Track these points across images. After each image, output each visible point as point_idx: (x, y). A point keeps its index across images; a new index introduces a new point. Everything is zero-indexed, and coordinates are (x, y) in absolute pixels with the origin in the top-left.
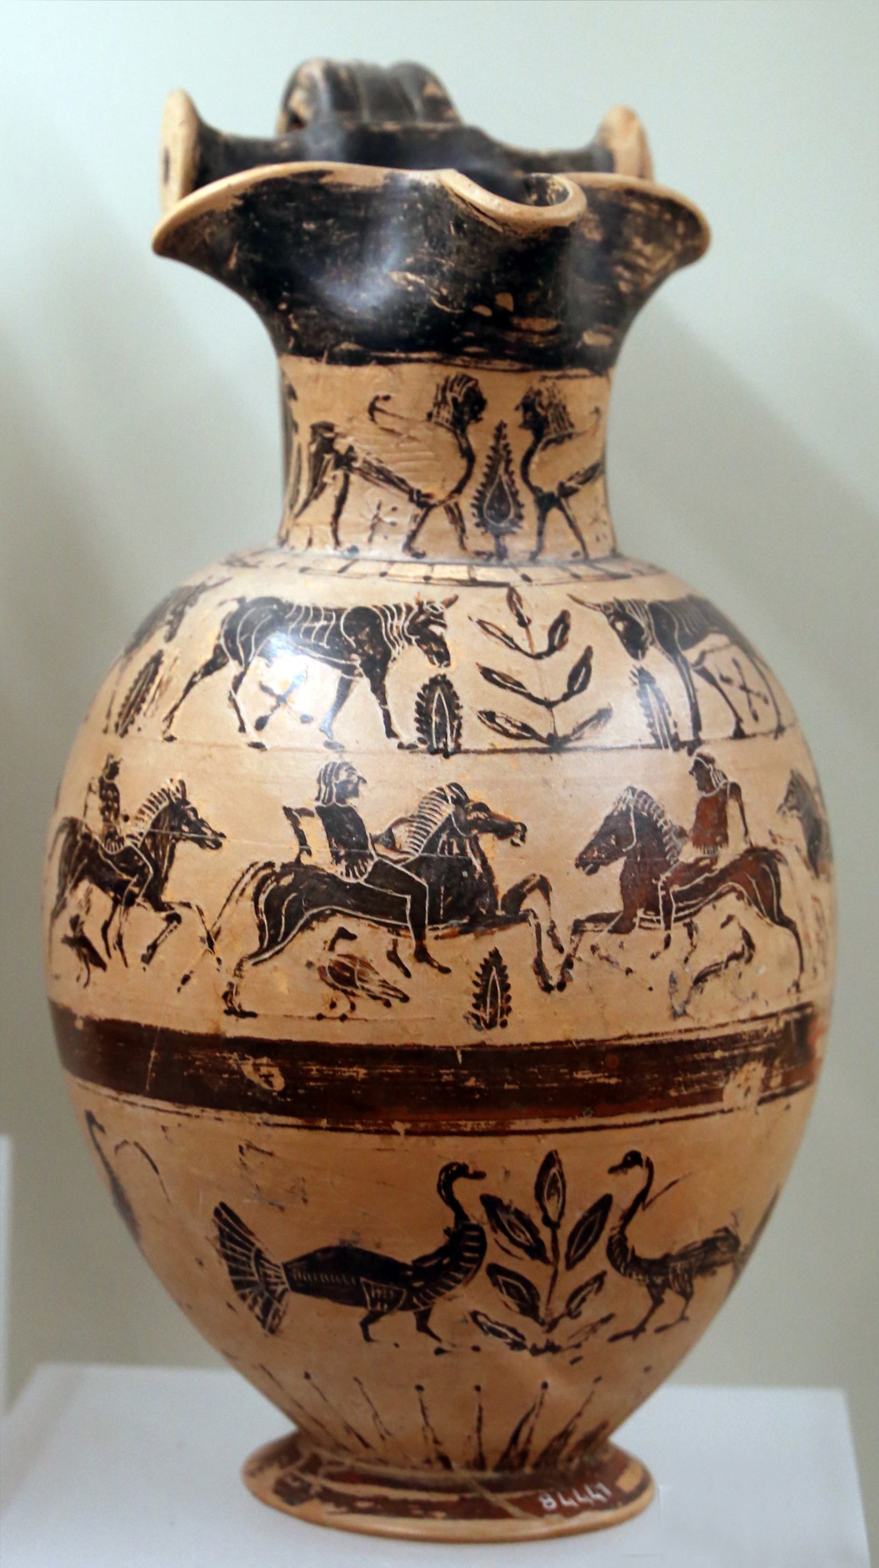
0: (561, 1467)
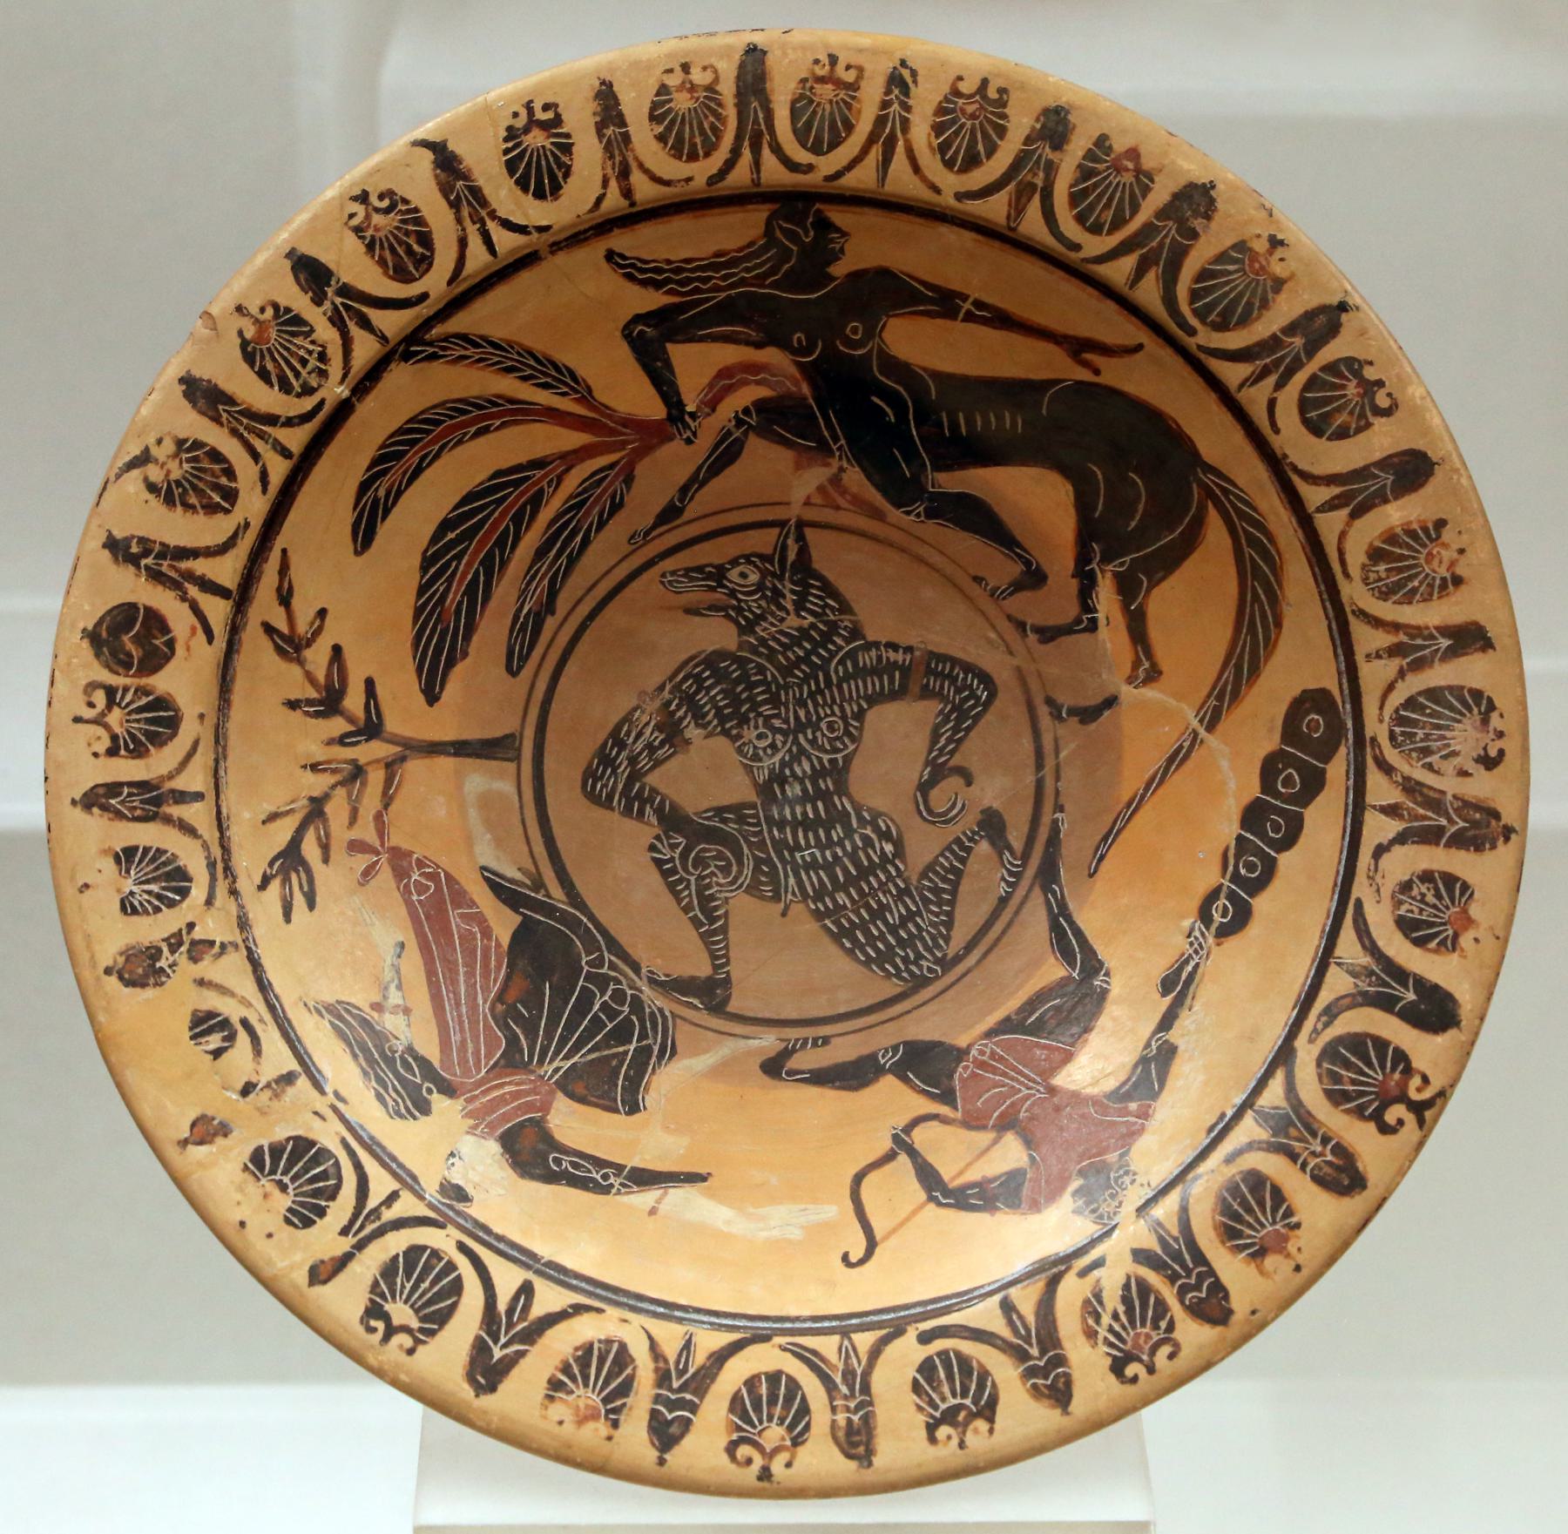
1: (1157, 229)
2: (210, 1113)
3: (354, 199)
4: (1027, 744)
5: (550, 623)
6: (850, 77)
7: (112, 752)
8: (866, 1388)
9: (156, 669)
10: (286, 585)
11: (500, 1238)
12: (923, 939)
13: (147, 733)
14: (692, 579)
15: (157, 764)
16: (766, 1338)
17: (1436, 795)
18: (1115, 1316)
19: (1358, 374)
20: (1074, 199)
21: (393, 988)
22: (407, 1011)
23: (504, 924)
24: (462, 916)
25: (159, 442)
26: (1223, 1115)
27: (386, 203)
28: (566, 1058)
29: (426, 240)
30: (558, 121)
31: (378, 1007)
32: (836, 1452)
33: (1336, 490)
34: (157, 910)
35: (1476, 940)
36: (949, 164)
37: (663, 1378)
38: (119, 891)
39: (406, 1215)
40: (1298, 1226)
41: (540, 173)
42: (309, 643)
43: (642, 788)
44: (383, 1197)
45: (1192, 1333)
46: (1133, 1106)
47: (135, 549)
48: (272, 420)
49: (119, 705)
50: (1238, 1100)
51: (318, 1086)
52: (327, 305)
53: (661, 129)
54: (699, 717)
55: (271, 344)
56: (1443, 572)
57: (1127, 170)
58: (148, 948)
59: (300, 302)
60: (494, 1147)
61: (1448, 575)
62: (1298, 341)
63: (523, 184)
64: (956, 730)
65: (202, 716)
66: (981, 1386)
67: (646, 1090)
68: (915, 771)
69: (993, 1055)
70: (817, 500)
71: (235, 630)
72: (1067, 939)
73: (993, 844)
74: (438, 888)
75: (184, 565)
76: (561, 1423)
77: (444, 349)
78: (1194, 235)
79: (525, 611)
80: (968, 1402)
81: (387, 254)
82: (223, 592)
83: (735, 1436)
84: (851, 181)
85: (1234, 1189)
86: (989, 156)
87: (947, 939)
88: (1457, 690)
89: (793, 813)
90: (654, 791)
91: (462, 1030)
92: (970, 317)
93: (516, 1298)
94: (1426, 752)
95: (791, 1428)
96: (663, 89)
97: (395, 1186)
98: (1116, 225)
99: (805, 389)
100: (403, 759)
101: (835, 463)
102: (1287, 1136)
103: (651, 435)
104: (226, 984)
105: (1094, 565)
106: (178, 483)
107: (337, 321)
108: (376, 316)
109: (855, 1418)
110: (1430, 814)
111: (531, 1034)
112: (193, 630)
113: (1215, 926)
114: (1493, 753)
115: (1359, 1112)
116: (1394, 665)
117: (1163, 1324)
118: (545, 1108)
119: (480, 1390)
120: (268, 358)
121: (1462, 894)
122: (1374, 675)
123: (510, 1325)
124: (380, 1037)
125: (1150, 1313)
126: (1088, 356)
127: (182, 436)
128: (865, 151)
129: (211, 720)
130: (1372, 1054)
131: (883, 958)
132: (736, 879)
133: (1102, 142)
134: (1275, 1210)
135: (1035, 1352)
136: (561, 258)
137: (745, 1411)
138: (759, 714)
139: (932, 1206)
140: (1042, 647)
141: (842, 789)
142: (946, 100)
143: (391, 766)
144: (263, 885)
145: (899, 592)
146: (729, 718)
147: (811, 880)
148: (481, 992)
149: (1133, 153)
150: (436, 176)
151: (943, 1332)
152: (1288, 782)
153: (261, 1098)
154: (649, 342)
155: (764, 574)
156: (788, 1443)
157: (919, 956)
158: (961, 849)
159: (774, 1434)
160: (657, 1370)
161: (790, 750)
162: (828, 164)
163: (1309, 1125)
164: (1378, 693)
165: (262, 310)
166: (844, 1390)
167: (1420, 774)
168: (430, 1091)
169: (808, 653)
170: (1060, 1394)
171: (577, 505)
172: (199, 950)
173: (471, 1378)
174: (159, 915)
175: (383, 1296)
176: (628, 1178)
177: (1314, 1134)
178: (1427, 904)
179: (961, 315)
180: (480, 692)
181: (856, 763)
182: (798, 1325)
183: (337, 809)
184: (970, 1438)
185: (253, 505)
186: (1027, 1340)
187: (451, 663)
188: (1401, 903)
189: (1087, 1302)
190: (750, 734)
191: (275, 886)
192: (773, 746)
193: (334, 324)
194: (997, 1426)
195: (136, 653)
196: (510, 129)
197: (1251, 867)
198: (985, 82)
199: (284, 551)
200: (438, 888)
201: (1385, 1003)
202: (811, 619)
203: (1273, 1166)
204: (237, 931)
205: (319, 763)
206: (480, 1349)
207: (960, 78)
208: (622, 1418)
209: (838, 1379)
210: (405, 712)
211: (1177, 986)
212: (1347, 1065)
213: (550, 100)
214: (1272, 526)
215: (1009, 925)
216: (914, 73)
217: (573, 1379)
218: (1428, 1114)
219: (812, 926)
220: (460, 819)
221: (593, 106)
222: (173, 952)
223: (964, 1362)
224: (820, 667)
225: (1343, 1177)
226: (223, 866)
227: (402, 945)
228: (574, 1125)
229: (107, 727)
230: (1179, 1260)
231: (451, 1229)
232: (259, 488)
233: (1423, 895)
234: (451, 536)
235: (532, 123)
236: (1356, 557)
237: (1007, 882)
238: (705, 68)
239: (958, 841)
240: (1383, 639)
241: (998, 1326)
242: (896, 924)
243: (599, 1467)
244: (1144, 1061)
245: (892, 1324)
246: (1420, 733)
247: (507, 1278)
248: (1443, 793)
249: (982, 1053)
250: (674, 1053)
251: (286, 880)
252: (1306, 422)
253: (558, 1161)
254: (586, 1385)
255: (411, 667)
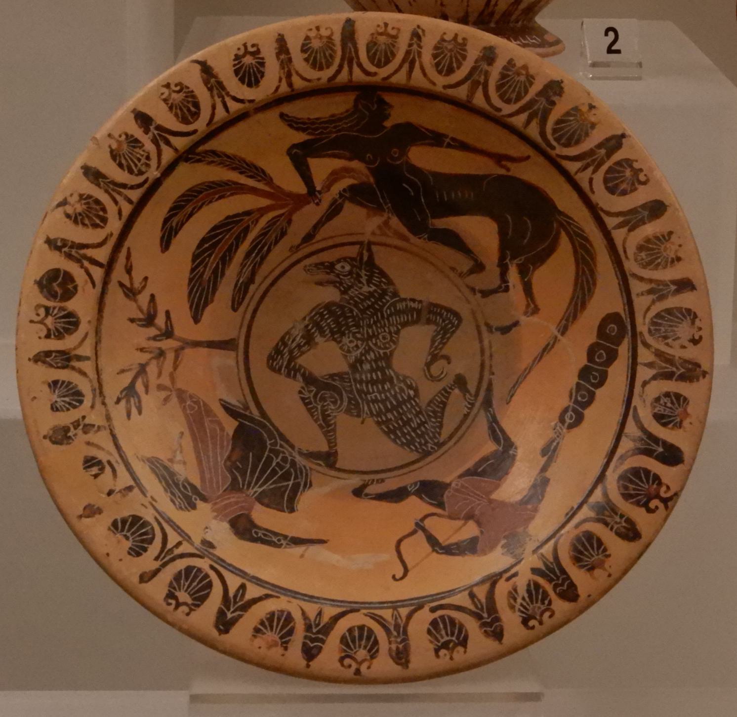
0: (511, 25)
1: (536, 101)
2: (92, 503)
3: (164, 86)
4: (477, 346)
5: (252, 288)
6: (393, 33)
7: (48, 336)
8: (405, 632)
9: (69, 298)
10: (129, 265)
11: (230, 565)
12: (428, 434)
13: (64, 328)
14: (319, 269)
15: (68, 343)
16: (357, 610)
17: (671, 357)
18: (523, 599)
19: (631, 166)
20: (499, 87)
21: (178, 452)
22: (185, 463)
23: (230, 425)
24: (210, 421)
25: (71, 195)
26: (573, 508)
27: (178, 88)
28: (260, 487)
29: (196, 105)
30: (258, 51)
31: (171, 460)
32: (391, 661)
33: (621, 219)
34: (68, 410)
35: (691, 423)
36: (440, 72)
37: (308, 628)
38: (50, 400)
39: (185, 552)
40: (609, 556)
41: (250, 75)
42: (140, 292)
43: (295, 365)
44: (175, 544)
45: (560, 606)
46: (529, 507)
47: (59, 244)
48: (124, 186)
49: (51, 315)
50: (580, 500)
51: (144, 493)
52: (150, 134)
53: (306, 56)
54: (322, 333)
55: (124, 152)
56: (672, 255)
57: (523, 74)
58: (63, 427)
59: (137, 132)
60: (226, 525)
61: (674, 257)
62: (603, 151)
63: (242, 80)
64: (442, 338)
65: (89, 322)
66: (460, 632)
67: (298, 503)
68: (423, 357)
69: (463, 486)
70: (378, 232)
71: (105, 283)
72: (496, 432)
73: (461, 390)
74: (199, 407)
75: (82, 252)
76: (260, 648)
77: (204, 157)
78: (553, 103)
79: (240, 282)
80: (454, 638)
81: (179, 111)
82: (99, 265)
83: (343, 654)
84: (394, 80)
85: (578, 539)
86: (459, 68)
87: (440, 434)
88: (680, 309)
89: (366, 377)
90: (300, 366)
91: (211, 473)
92: (449, 146)
93: (238, 591)
94: (666, 338)
95: (369, 651)
96: (307, 38)
97: (180, 539)
98: (519, 98)
99: (372, 180)
100: (182, 348)
101: (386, 215)
102: (603, 515)
103: (299, 201)
104: (99, 444)
105: (507, 261)
106: (80, 214)
107: (155, 141)
108: (174, 140)
109: (401, 646)
110: (668, 366)
111: (244, 475)
112: (86, 281)
113: (566, 425)
114: (697, 337)
115: (638, 503)
116: (651, 297)
117: (546, 602)
118: (250, 509)
119: (221, 632)
120: (122, 158)
121: (684, 402)
122: (641, 303)
123: (235, 602)
124: (172, 474)
125: (540, 597)
126: (504, 163)
127: (82, 192)
128: (401, 67)
129: (95, 323)
130: (643, 475)
131: (409, 444)
132: (340, 407)
133: (511, 62)
134: (599, 548)
135: (485, 615)
136: (260, 116)
137: (348, 643)
138: (350, 332)
139: (435, 554)
140: (484, 300)
141: (389, 366)
142: (439, 42)
143: (178, 352)
144: (118, 401)
145: (415, 274)
146: (336, 333)
147: (375, 408)
148: (220, 454)
149: (525, 67)
150: (202, 77)
151: (442, 607)
152: (600, 356)
153: (116, 497)
154: (300, 156)
155: (353, 266)
156: (368, 658)
157: (426, 442)
158: (446, 392)
159: (362, 654)
160: (305, 624)
161: (365, 348)
162: (384, 72)
163: (614, 510)
164: (642, 313)
165: (120, 136)
166: (395, 633)
167: (663, 348)
168: (196, 499)
169: (373, 304)
170: (498, 635)
171: (264, 234)
172: (87, 428)
173: (217, 626)
174: (69, 412)
175: (174, 588)
176: (289, 541)
177: (616, 514)
178: (668, 407)
179: (445, 144)
180: (220, 318)
181: (396, 354)
182: (372, 605)
183: (152, 369)
184: (455, 655)
185: (115, 225)
186: (482, 609)
187: (206, 304)
188: (655, 407)
189: (510, 592)
190: (345, 340)
191: (123, 403)
192: (357, 346)
193: (154, 143)
194: (468, 650)
195: (59, 291)
196: (236, 55)
197: (583, 397)
198: (456, 35)
199: (129, 249)
200: (199, 407)
201: (648, 452)
202: (374, 288)
203: (598, 529)
204: (105, 421)
205: (144, 348)
206: (221, 614)
207: (445, 33)
208: (288, 645)
209: (392, 628)
210: (184, 327)
211: (549, 451)
212: (631, 481)
213: (255, 42)
214: (591, 239)
215: (468, 427)
216: (423, 31)
217: (266, 627)
218: (669, 504)
219: (375, 429)
220: (211, 378)
221: (275, 45)
222: (75, 428)
223: (452, 621)
224: (378, 310)
225: (631, 533)
226: (99, 390)
227: (182, 433)
228: (265, 517)
229: (45, 325)
230: (553, 572)
231: (206, 559)
232: (117, 216)
233: (666, 403)
234: (207, 245)
235: (247, 52)
236: (631, 250)
237: (467, 407)
238: (326, 29)
239: (444, 389)
240: (646, 287)
241: (467, 603)
242: (415, 427)
243: (278, 669)
244: (534, 486)
245: (418, 605)
246: (663, 329)
247: (234, 582)
248: (674, 356)
249: (457, 485)
250: (311, 485)
251: (128, 402)
252: (607, 188)
253: (256, 533)
254: (272, 629)
255: (187, 306)
